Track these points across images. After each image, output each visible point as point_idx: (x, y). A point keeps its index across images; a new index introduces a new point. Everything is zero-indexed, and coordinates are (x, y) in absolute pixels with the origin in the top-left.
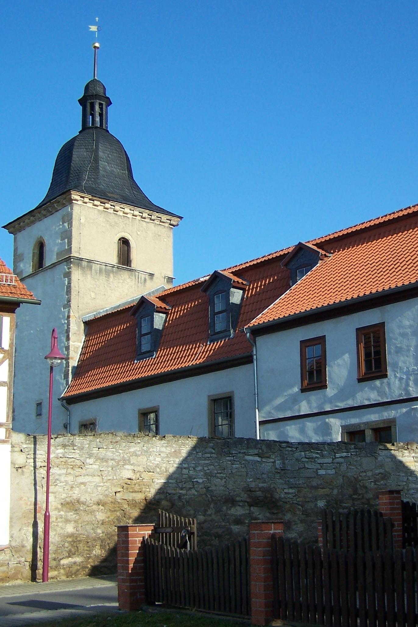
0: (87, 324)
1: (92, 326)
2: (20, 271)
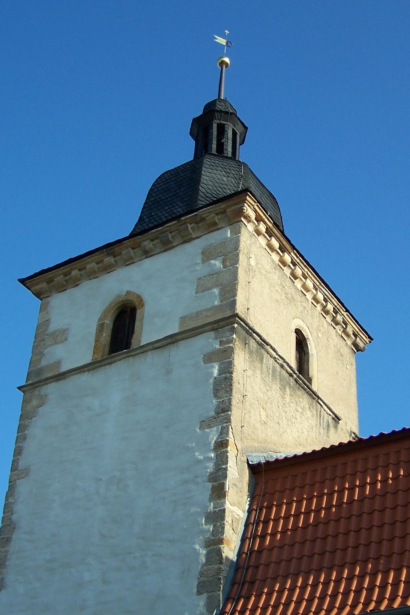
0: (255, 470)
1: (266, 475)
2: (52, 361)
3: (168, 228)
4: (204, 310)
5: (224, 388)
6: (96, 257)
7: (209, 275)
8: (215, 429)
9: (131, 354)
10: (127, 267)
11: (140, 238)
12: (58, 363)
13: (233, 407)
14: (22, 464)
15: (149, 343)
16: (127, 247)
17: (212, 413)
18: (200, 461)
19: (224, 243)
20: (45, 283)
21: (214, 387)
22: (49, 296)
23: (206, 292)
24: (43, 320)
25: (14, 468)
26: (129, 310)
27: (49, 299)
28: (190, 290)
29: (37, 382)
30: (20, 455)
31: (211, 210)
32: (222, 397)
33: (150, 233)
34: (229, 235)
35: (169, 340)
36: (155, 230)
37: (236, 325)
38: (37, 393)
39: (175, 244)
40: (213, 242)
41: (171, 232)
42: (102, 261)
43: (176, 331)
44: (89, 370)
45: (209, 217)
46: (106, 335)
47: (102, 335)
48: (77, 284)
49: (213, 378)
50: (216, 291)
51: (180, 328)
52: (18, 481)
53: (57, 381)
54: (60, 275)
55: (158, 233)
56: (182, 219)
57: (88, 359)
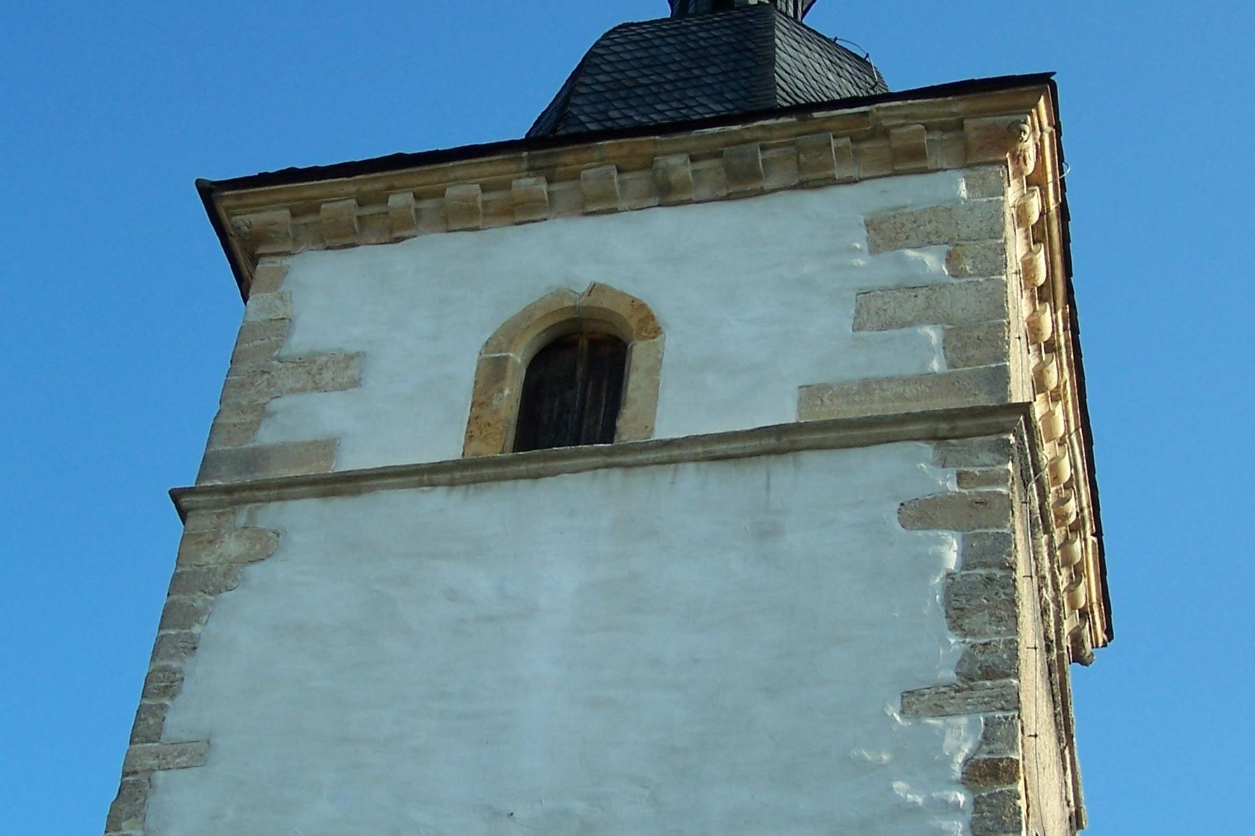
2: (305, 435)
3: (759, 134)
4: (890, 380)
5: (987, 607)
6: (486, 169)
7: (898, 288)
8: (963, 720)
9: (617, 459)
10: (590, 220)
11: (656, 142)
12: (328, 446)
13: (1022, 668)
14: (180, 720)
15: (697, 437)
16: (603, 161)
17: (949, 675)
18: (913, 809)
19: (948, 210)
20: (288, 212)
21: (947, 602)
22: (288, 254)
23: (896, 332)
24: (264, 316)
25: (146, 727)
26: (584, 343)
27: (287, 261)
28: (832, 321)
29: (250, 487)
30: (173, 697)
31: (916, 111)
32: (981, 633)
33: (696, 133)
34: (963, 192)
35: (772, 442)
36: (716, 129)
37: (1012, 438)
38: (242, 519)
39: (768, 185)
40: (909, 202)
41: (763, 148)
42: (507, 186)
43: (791, 418)
44: (452, 484)
45: (904, 130)
46: (510, 394)
47: (501, 391)
48: (397, 234)
49: (943, 574)
50: (933, 334)
51: (800, 414)
52: (160, 774)
53: (324, 495)
54: (349, 196)
55: (721, 140)
56: (816, 115)
57: (450, 448)
